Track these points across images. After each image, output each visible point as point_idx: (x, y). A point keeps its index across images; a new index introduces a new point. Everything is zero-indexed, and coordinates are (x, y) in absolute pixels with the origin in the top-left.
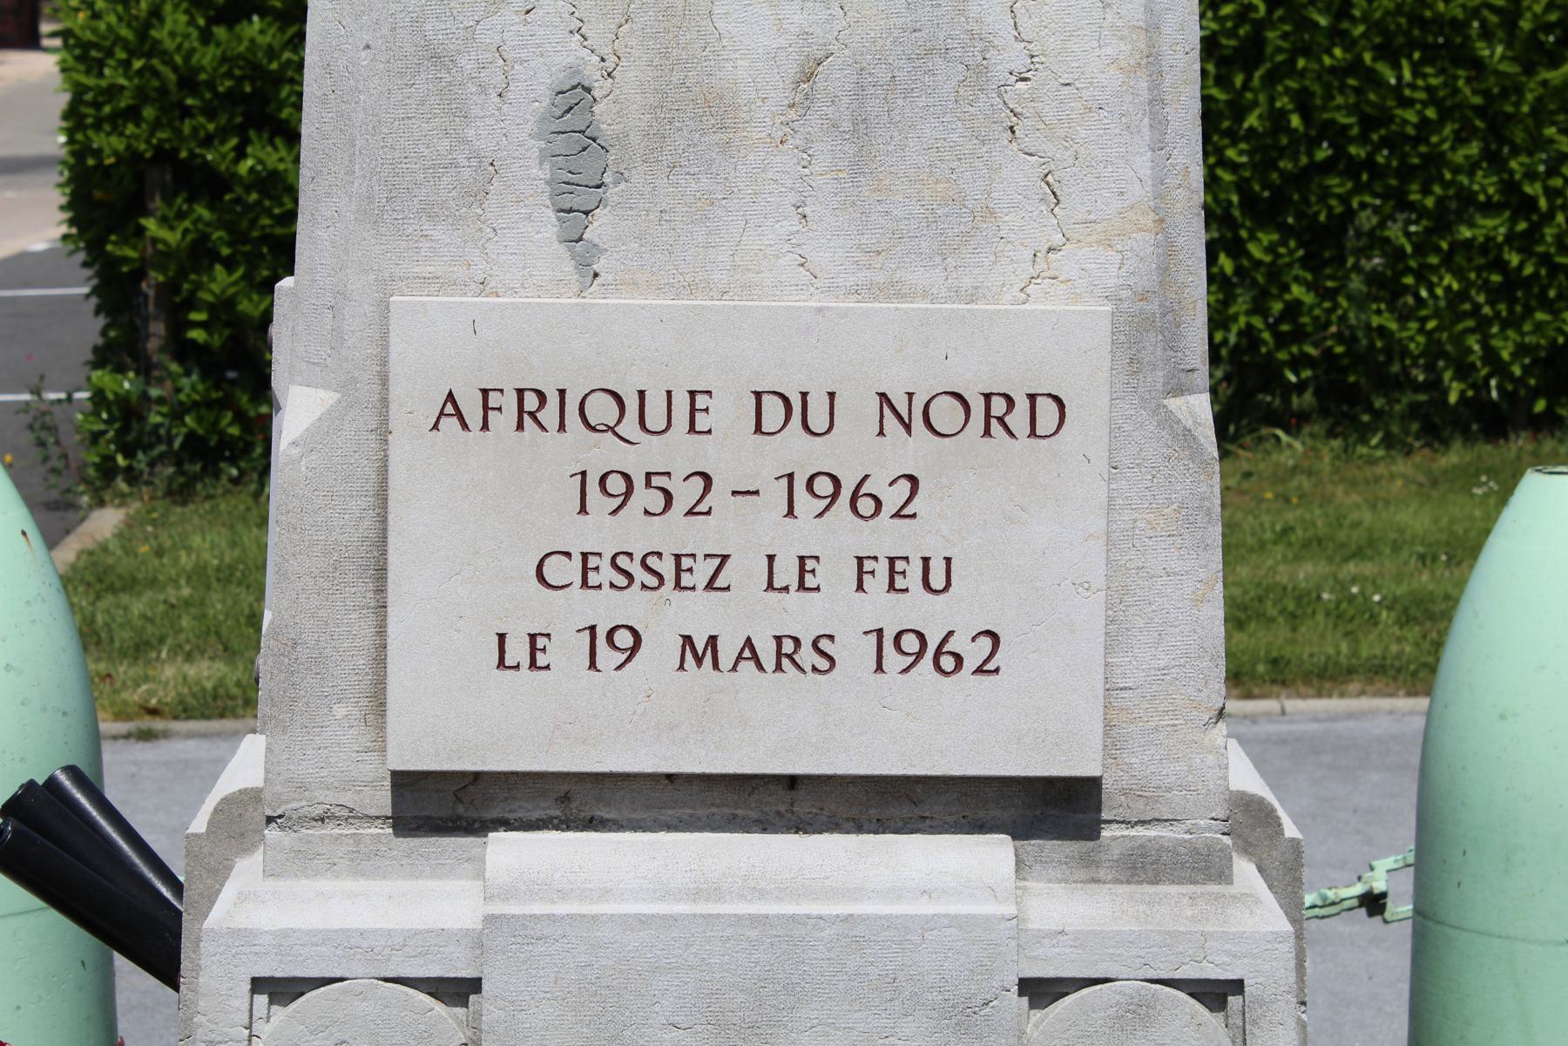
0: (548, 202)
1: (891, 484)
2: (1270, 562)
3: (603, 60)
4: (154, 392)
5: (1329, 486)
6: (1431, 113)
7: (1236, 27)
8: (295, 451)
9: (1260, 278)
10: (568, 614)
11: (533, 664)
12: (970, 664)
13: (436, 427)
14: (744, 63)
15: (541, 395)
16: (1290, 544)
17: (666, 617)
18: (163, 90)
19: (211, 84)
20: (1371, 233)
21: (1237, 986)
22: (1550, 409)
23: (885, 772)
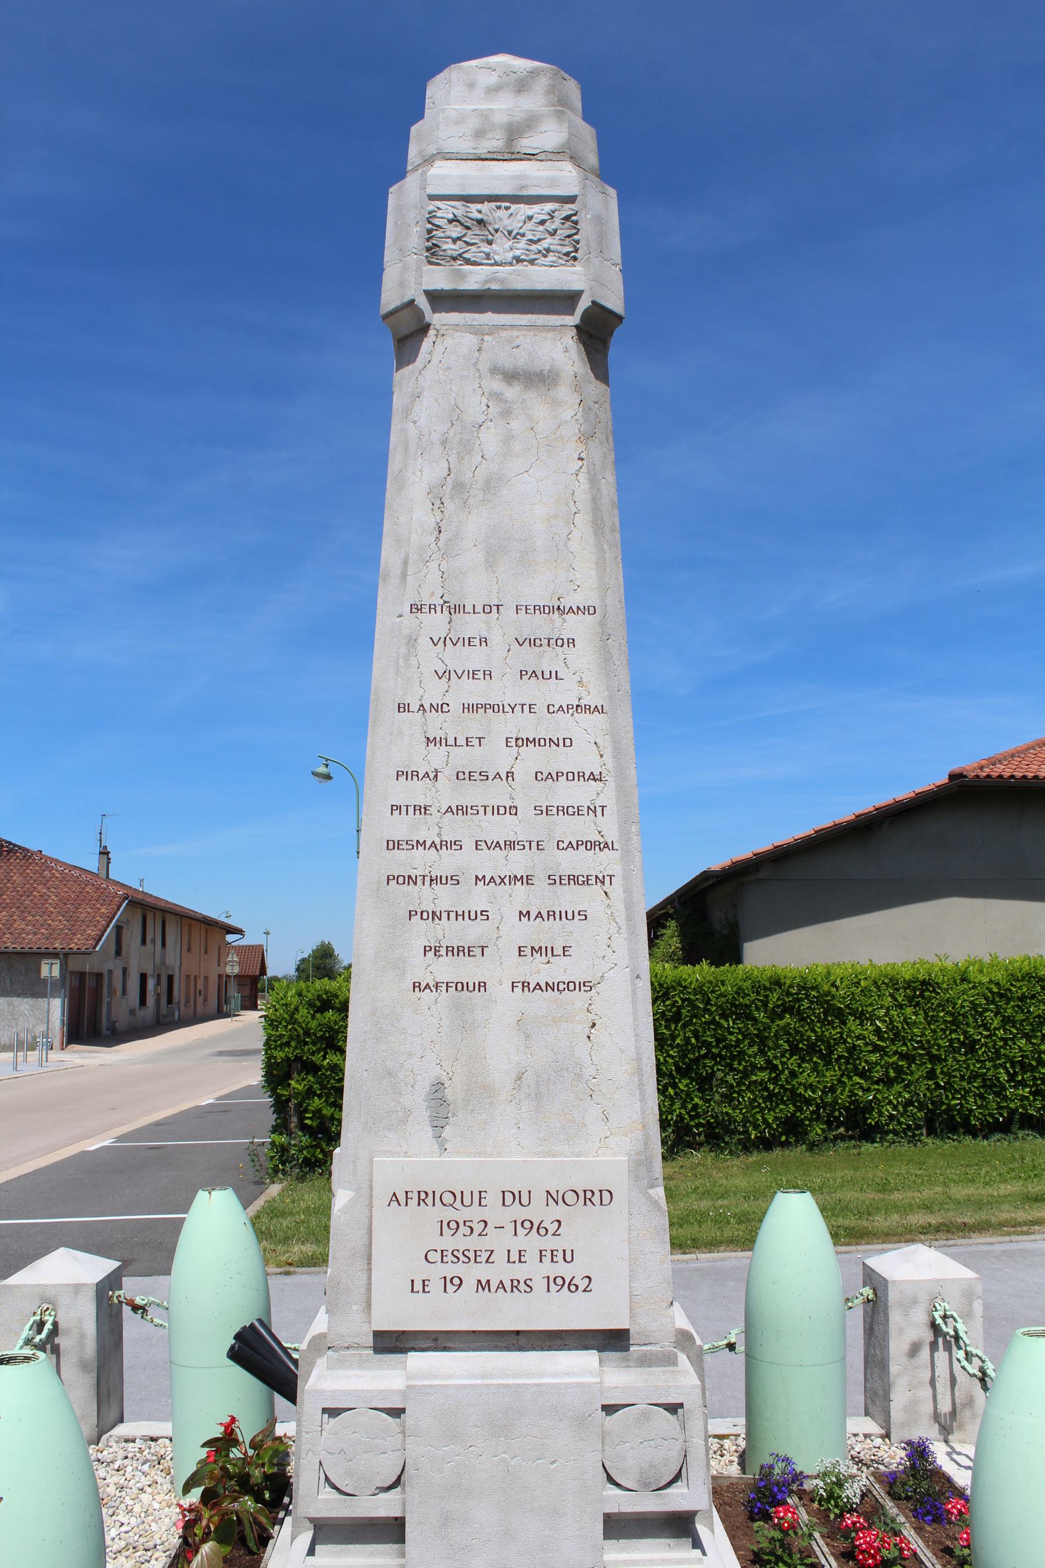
4: (293, 1142)
6: (740, 1037)
8: (339, 1213)
10: (437, 1272)
12: (581, 1288)
15: (426, 1193)
17: (472, 1273)
18: (298, 1036)
19: (315, 1034)
20: (721, 1079)
21: (681, 1405)
22: (787, 1139)
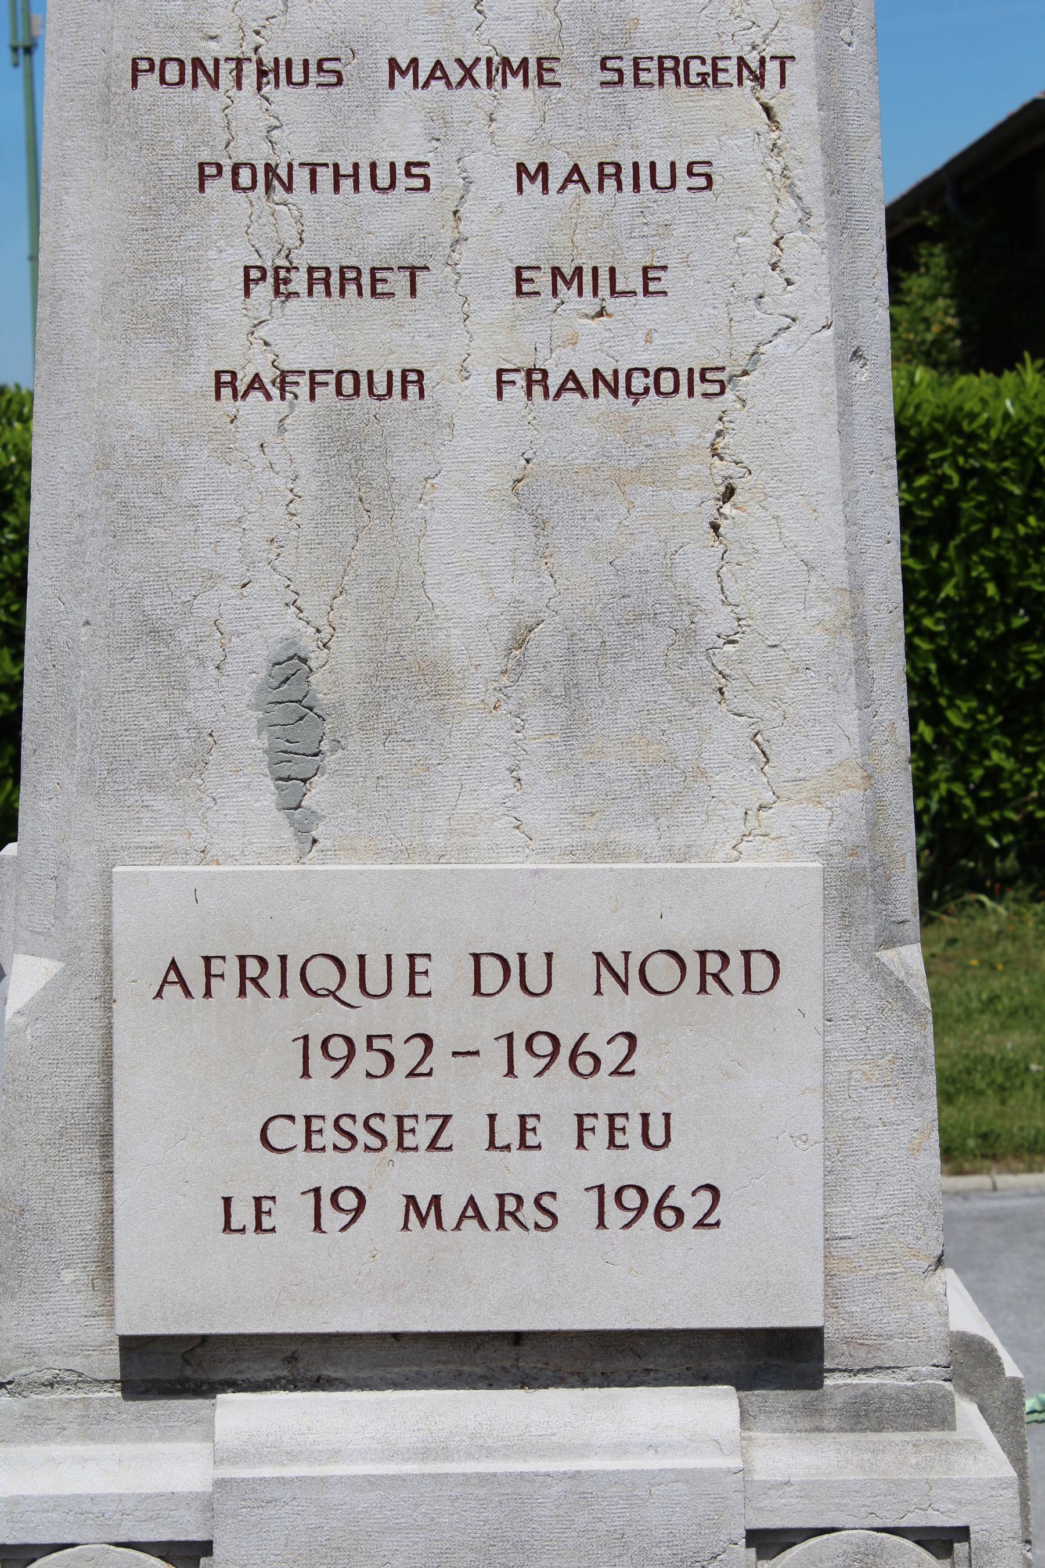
0: (267, 771)
1: (609, 1043)
2: (977, 1032)
3: (318, 631)
5: (1034, 951)
7: (931, 498)
8: (21, 1021)
9: (960, 745)
10: (294, 1175)
11: (259, 1227)
12: (691, 1217)
13: (159, 994)
14: (457, 632)
15: (263, 962)
16: (997, 1013)
17: (391, 1178)
21: (963, 1533)
23: (609, 1327)
